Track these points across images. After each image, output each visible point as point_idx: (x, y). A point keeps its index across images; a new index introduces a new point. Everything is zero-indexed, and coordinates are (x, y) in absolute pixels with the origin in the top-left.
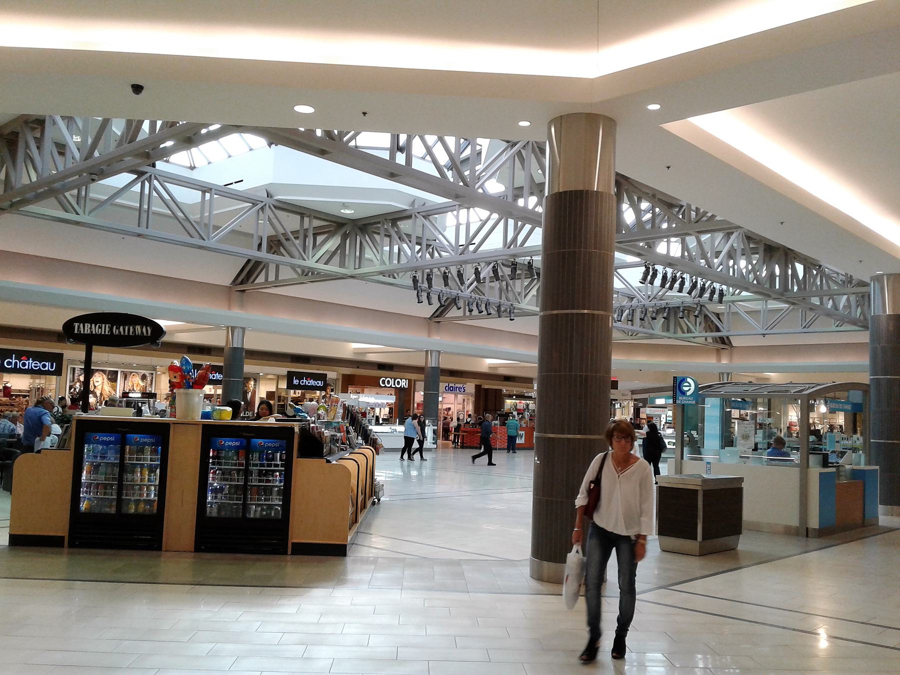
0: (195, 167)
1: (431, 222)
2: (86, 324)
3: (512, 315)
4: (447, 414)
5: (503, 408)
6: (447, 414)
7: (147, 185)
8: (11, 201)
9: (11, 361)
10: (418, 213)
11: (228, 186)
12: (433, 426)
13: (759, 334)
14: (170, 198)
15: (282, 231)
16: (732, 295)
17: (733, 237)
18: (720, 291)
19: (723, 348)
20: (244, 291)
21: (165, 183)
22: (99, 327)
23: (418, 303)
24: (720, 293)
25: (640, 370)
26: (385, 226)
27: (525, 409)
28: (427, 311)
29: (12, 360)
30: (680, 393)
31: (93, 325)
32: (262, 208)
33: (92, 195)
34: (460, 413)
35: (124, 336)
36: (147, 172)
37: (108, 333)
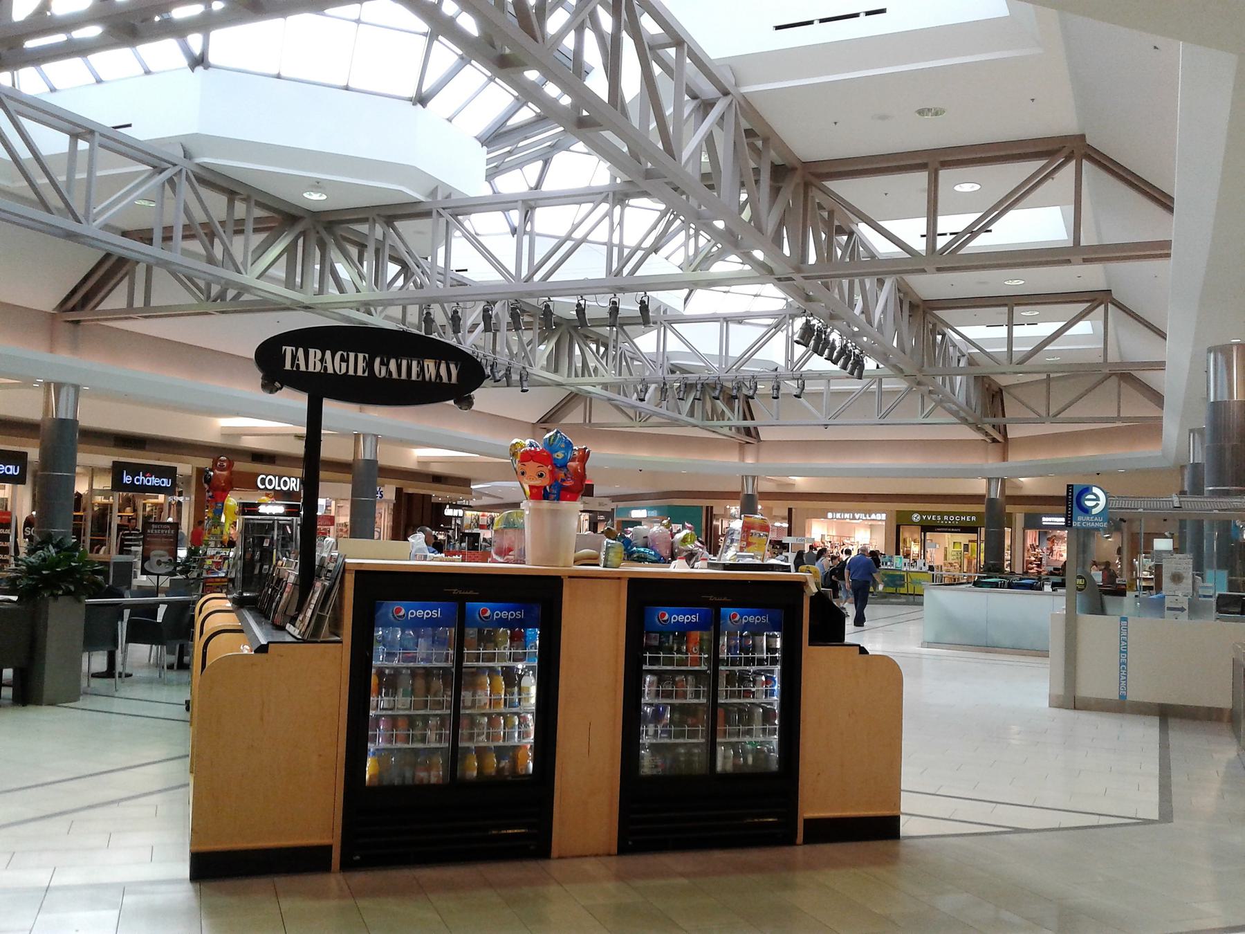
2: (312, 351)
3: (525, 384)
10: (444, 209)
13: (819, 425)
20: (78, 322)
22: (342, 359)
25: (641, 471)
27: (489, 525)
31: (328, 353)
35: (399, 381)
37: (364, 372)
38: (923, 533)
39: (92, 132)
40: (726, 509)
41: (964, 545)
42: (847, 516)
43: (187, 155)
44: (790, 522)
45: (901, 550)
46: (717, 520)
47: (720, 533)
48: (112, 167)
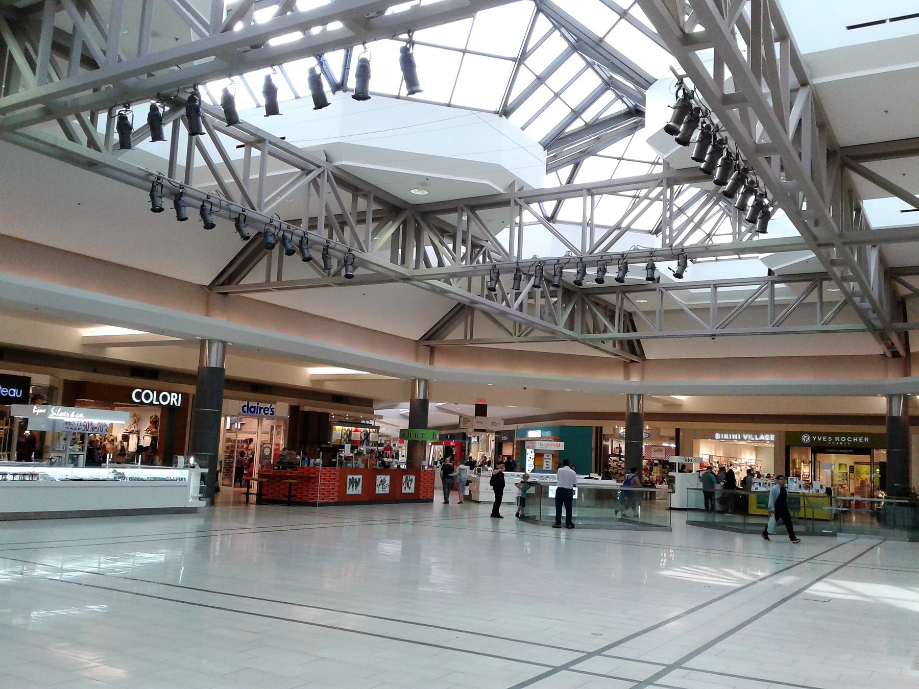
4: (248, 447)
5: (330, 439)
6: (248, 447)
10: (520, 198)
12: (201, 467)
20: (226, 294)
27: (363, 441)
34: (264, 446)
38: (813, 454)
40: (615, 429)
41: (850, 466)
42: (735, 436)
43: (328, 159)
44: (677, 443)
45: (791, 472)
46: (607, 440)
47: (610, 453)
48: (278, 169)
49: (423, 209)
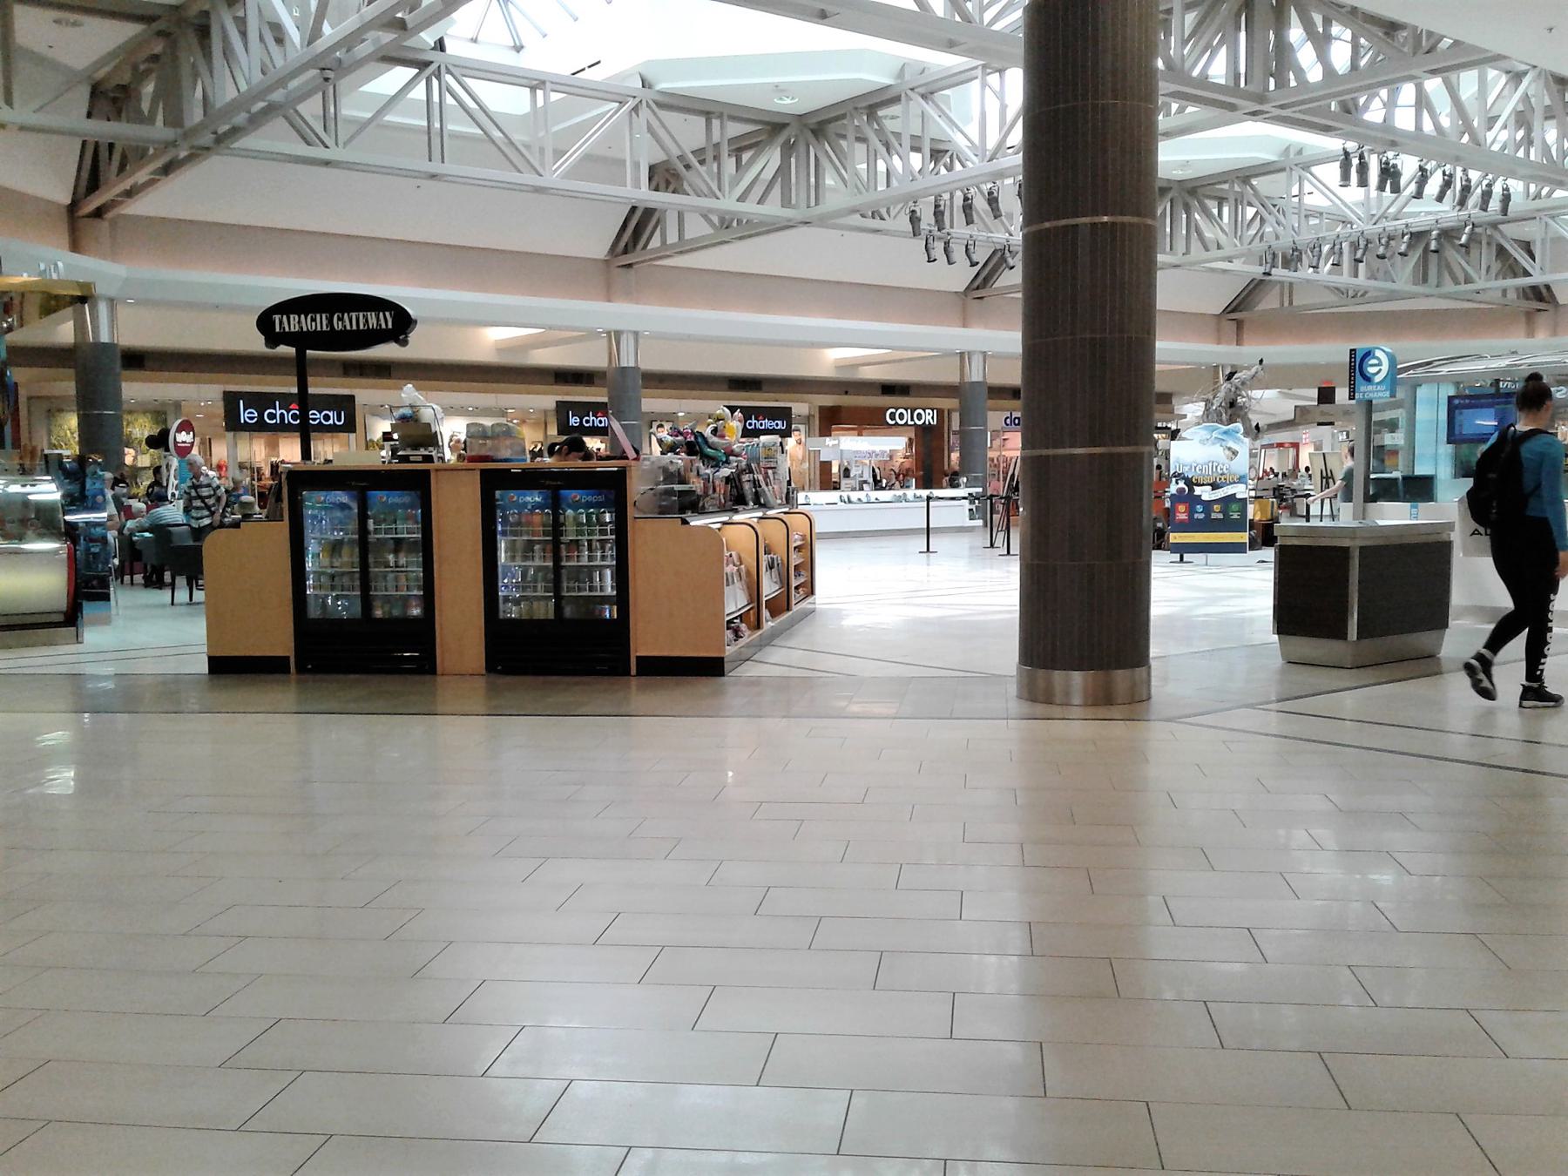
0: (522, 47)
1: (938, 106)
2: (292, 316)
7: (435, 82)
8: (215, 133)
9: (274, 411)
10: (912, 89)
11: (576, 76)
14: (476, 107)
15: (675, 152)
16: (1533, 200)
17: (1526, 81)
18: (1503, 190)
19: (1539, 310)
20: (630, 266)
21: (464, 78)
23: (929, 261)
24: (1503, 194)
26: (855, 121)
28: (959, 276)
29: (275, 409)
30: (1361, 378)
31: (303, 316)
32: (635, 109)
33: (346, 112)
35: (351, 331)
36: (432, 62)
37: (327, 327)
39: (544, 82)
43: (645, 84)
49: (1190, 185)
